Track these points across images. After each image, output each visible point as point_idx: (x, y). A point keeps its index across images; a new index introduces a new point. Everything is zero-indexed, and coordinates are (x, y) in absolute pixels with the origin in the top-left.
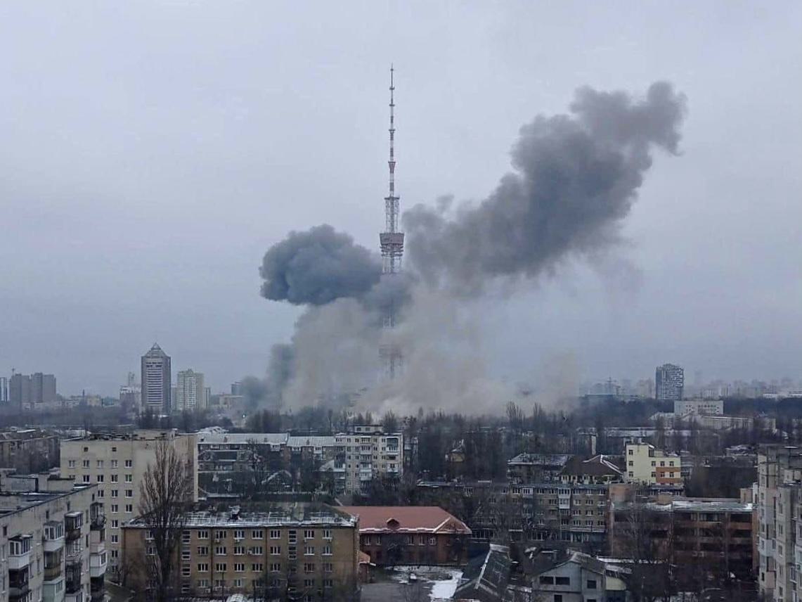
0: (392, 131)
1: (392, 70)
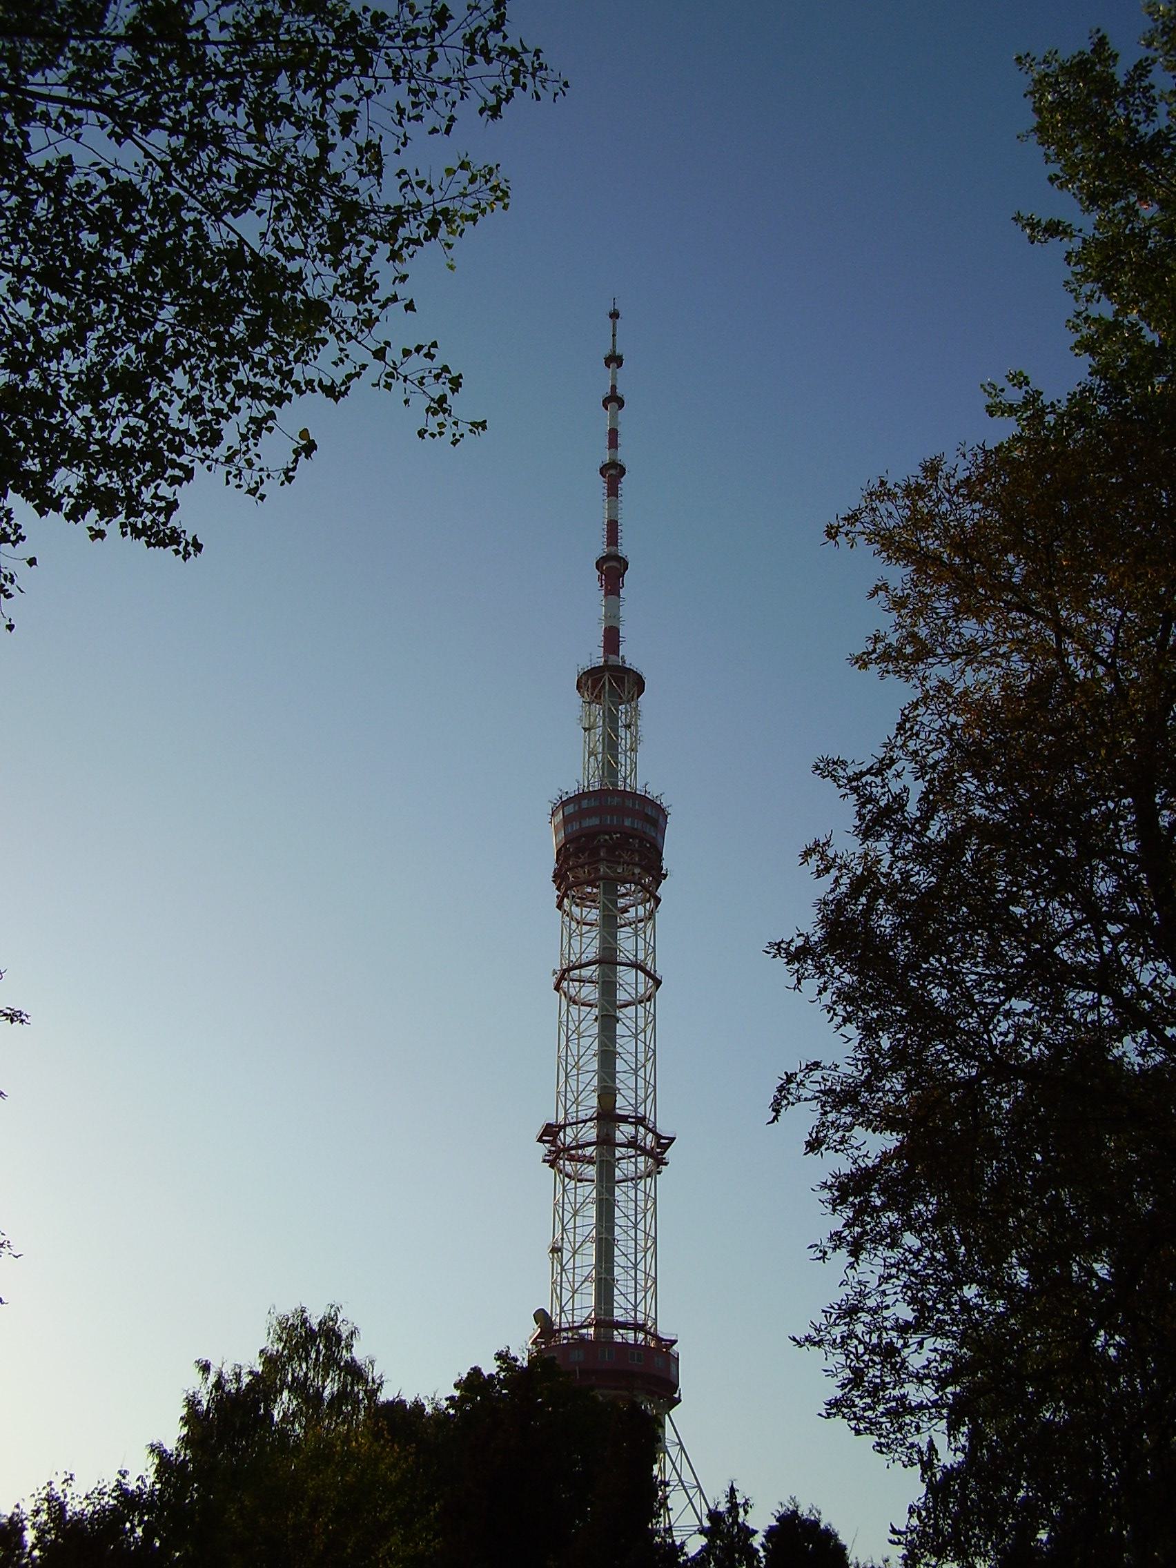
0: (613, 473)
1: (614, 315)
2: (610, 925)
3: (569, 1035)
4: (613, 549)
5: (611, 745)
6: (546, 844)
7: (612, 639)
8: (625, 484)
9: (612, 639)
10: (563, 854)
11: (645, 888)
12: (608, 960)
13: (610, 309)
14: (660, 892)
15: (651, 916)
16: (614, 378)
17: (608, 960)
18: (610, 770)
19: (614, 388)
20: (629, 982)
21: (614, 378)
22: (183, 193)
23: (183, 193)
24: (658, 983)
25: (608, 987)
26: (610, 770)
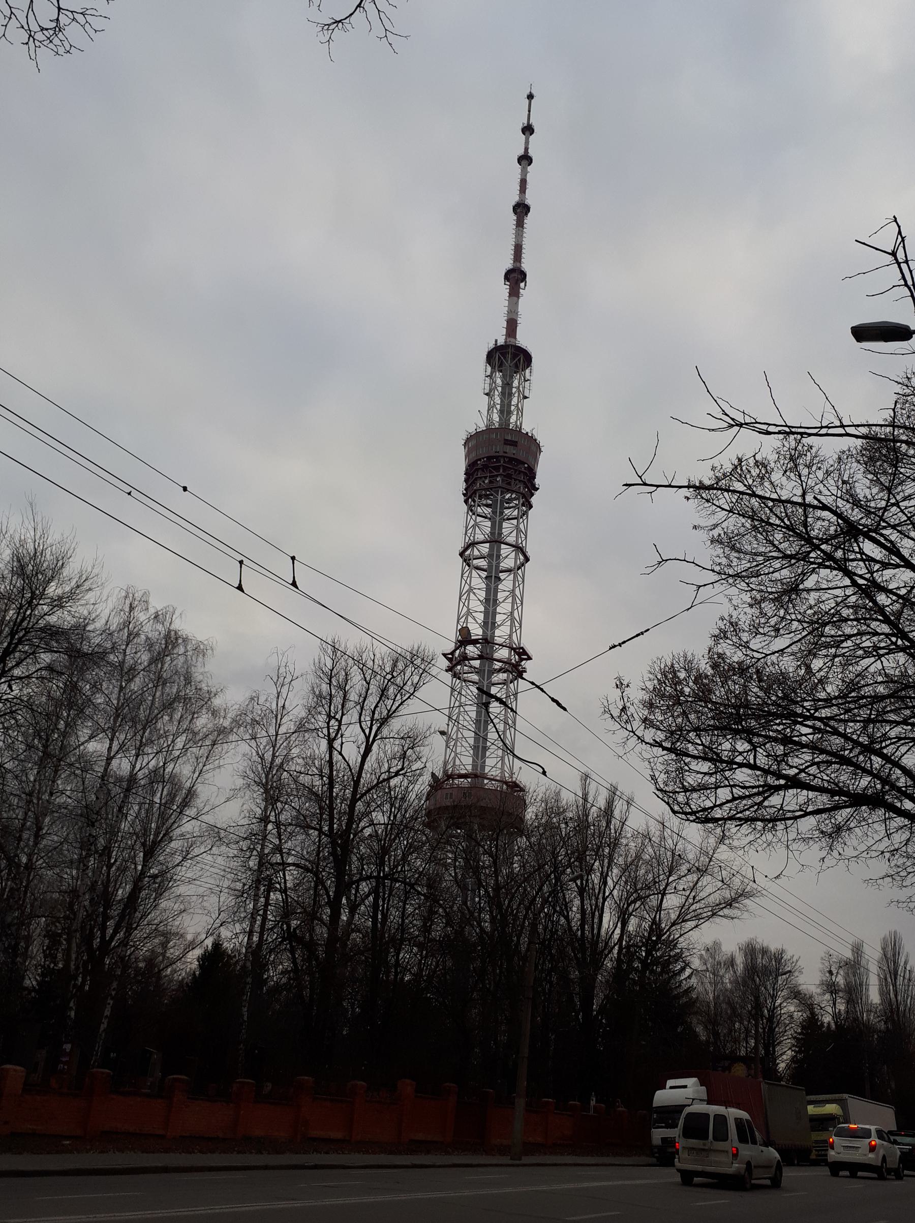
1: (530, 97)
2: (497, 522)
3: (466, 594)
4: (518, 264)
5: (507, 394)
6: (456, 465)
7: (512, 326)
8: (529, 220)
9: (512, 326)
10: (471, 474)
11: (524, 496)
12: (496, 540)
13: (528, 92)
14: (533, 500)
15: (525, 513)
16: (527, 142)
17: (496, 540)
18: (505, 411)
19: (526, 149)
20: (509, 559)
21: (527, 142)
22: (518, 1162)
23: (518, 1162)
24: (527, 559)
25: (494, 556)
26: (505, 411)
